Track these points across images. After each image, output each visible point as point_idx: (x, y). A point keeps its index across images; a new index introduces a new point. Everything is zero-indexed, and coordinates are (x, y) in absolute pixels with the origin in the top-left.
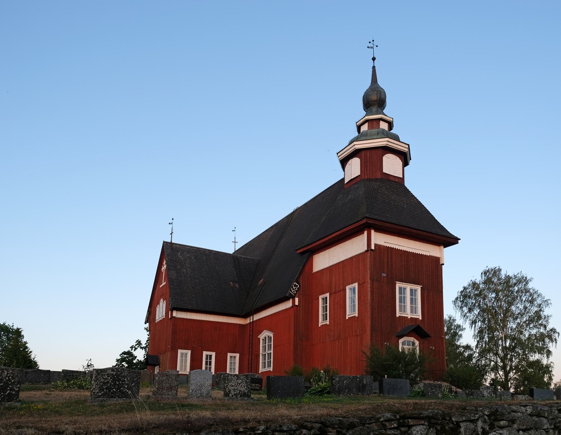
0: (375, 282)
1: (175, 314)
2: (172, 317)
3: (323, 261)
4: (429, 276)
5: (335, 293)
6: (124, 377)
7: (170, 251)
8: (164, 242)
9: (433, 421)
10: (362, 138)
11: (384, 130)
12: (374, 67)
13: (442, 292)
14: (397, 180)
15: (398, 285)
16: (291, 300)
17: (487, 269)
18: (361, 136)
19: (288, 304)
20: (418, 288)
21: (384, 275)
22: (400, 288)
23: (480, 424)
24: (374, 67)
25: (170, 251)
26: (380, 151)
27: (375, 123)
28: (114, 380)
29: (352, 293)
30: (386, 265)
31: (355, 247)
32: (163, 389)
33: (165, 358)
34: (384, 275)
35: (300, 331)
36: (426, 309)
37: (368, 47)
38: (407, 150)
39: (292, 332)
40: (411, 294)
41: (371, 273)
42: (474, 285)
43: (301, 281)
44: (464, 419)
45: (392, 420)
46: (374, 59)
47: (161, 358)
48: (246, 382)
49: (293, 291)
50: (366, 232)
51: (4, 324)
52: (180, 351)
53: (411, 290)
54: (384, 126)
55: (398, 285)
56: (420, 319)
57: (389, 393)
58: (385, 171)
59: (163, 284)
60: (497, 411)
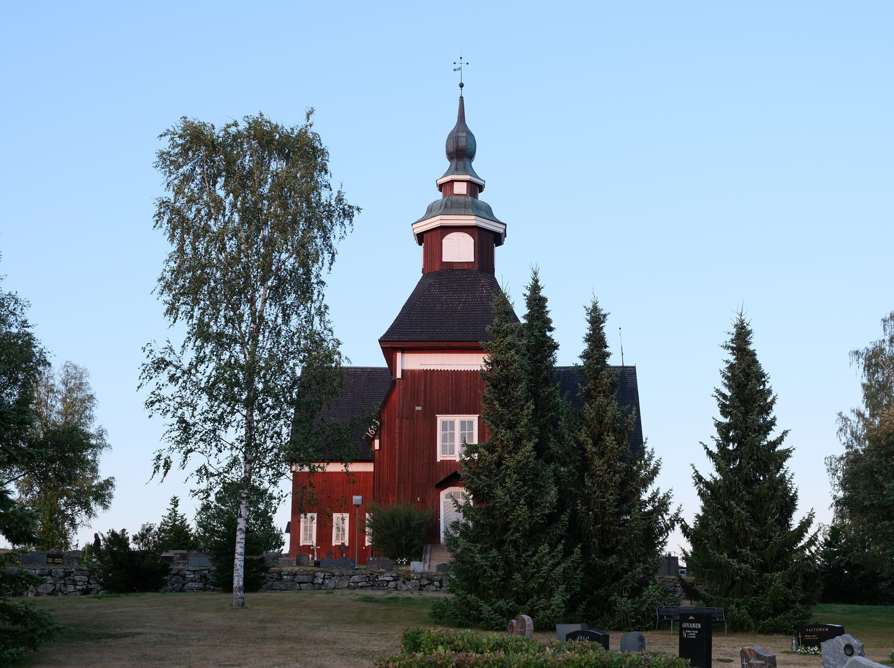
0: (404, 420)
10: (432, 214)
12: (462, 97)
14: (466, 267)
21: (418, 408)
24: (462, 97)
26: (439, 231)
30: (422, 395)
34: (418, 408)
37: (455, 70)
46: (462, 86)
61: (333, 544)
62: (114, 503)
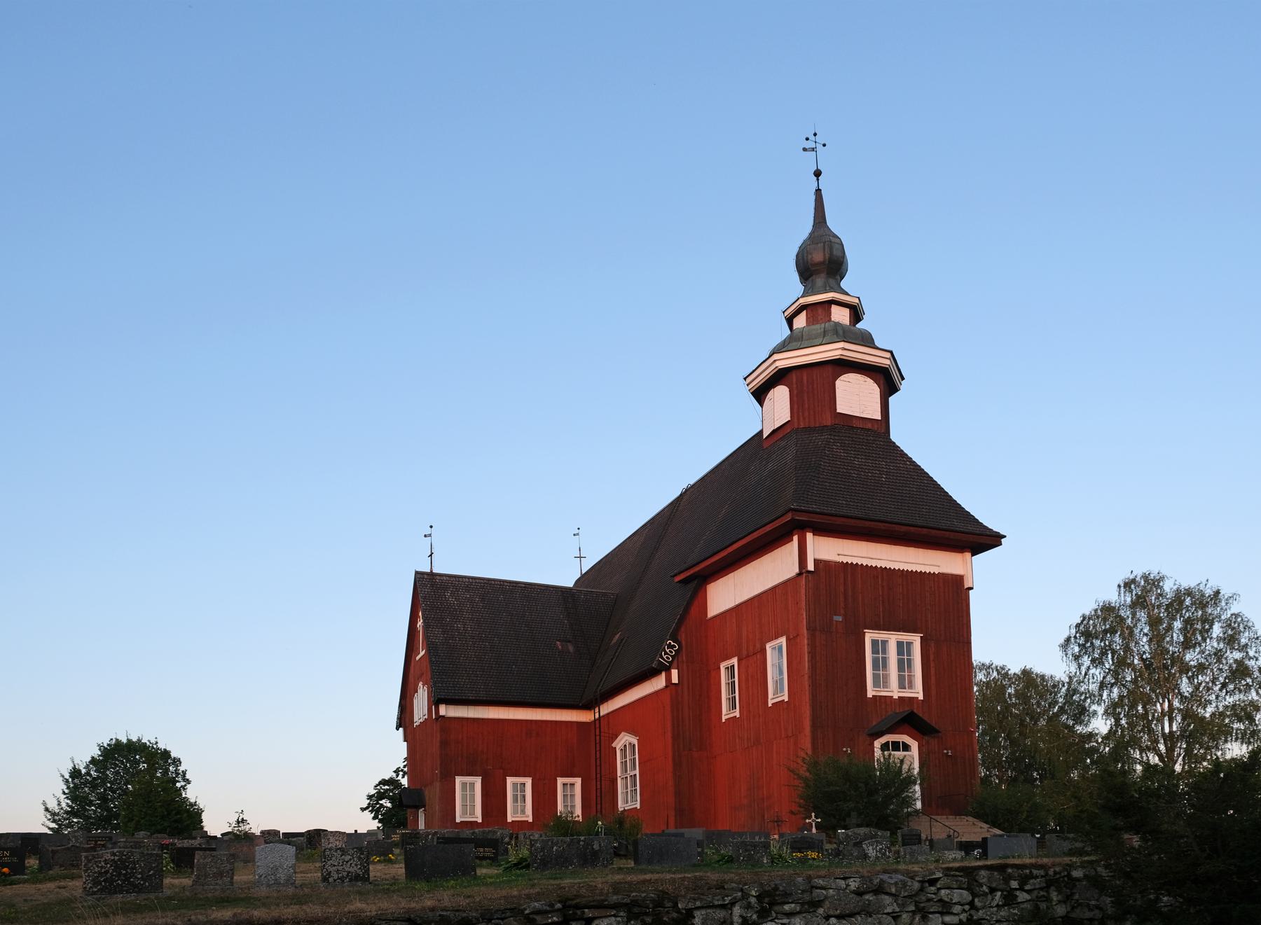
1: (443, 710)
2: (439, 717)
3: (725, 595)
4: (941, 615)
5: (748, 656)
6: (134, 863)
7: (433, 592)
8: (417, 573)
9: (636, 910)
11: (837, 324)
12: (818, 191)
13: (969, 643)
14: (869, 426)
15: (870, 636)
16: (663, 674)
17: (1132, 577)
18: (793, 341)
19: (658, 683)
20: (916, 640)
21: (840, 619)
22: (875, 643)
23: (737, 910)
24: (818, 191)
25: (433, 592)
26: (830, 368)
27: (820, 310)
28: (117, 868)
29: (776, 655)
30: (842, 599)
31: (777, 567)
32: (206, 876)
33: (433, 794)
34: (840, 619)
35: (686, 730)
36: (933, 678)
37: (805, 149)
38: (888, 362)
39: (669, 734)
40: (900, 652)
41: (809, 616)
42: (1107, 610)
43: (682, 637)
44: (698, 904)
45: (546, 912)
46: (818, 174)
47: (426, 793)
48: (359, 858)
49: (666, 658)
50: (796, 538)
51: (139, 740)
52: (459, 780)
53: (900, 645)
54: (840, 316)
55: (870, 636)
56: (921, 697)
57: (650, 862)
58: (842, 408)
59: (422, 653)
60: (776, 889)
61: (509, 820)
62: (1154, 569)
